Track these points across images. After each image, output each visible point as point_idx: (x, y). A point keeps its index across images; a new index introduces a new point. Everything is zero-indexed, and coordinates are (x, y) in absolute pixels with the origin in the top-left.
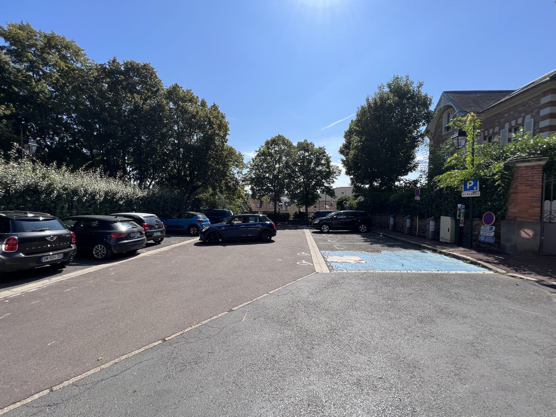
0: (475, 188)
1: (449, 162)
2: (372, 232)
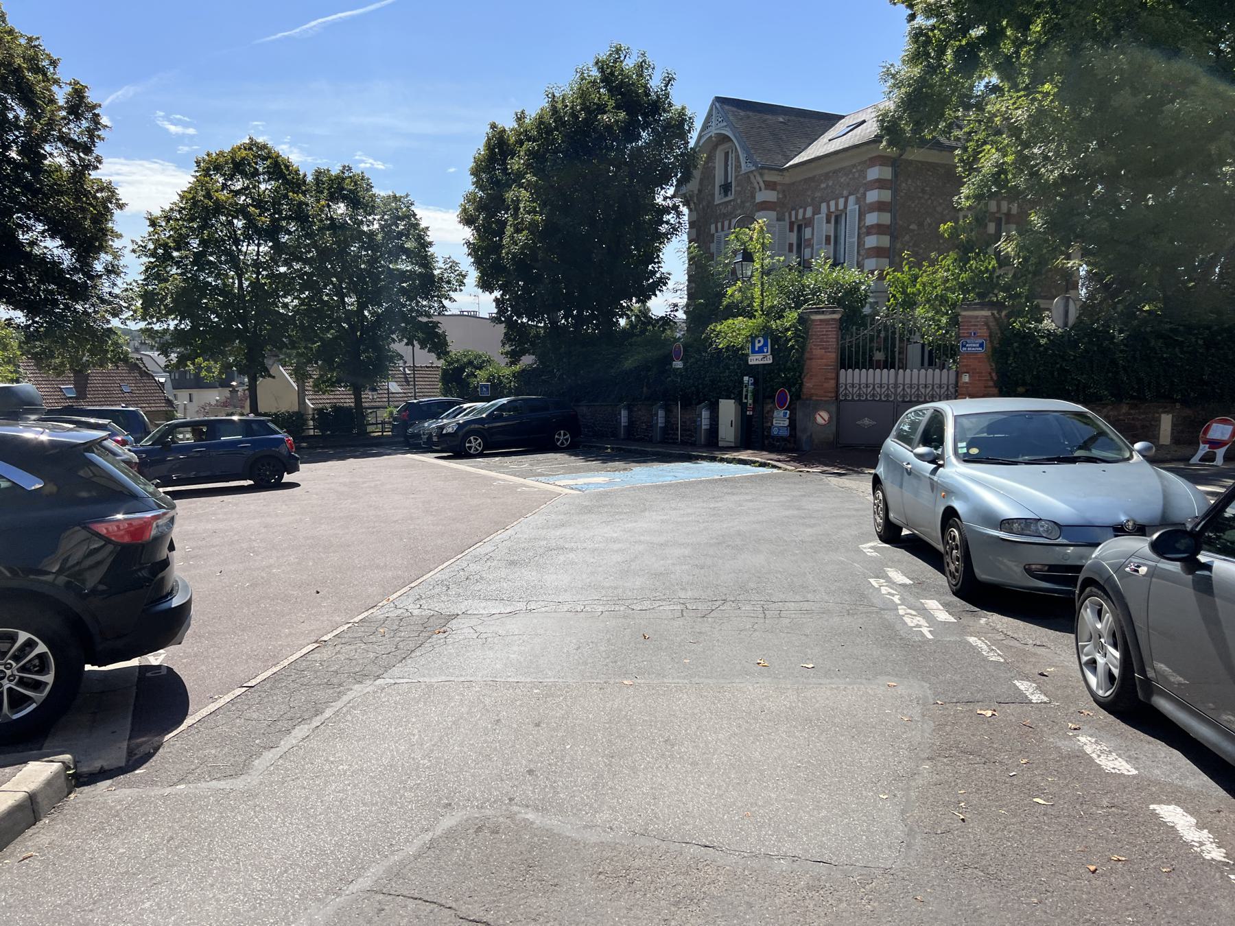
0: (765, 350)
1: (731, 296)
2: (585, 446)
